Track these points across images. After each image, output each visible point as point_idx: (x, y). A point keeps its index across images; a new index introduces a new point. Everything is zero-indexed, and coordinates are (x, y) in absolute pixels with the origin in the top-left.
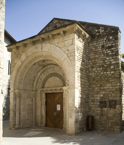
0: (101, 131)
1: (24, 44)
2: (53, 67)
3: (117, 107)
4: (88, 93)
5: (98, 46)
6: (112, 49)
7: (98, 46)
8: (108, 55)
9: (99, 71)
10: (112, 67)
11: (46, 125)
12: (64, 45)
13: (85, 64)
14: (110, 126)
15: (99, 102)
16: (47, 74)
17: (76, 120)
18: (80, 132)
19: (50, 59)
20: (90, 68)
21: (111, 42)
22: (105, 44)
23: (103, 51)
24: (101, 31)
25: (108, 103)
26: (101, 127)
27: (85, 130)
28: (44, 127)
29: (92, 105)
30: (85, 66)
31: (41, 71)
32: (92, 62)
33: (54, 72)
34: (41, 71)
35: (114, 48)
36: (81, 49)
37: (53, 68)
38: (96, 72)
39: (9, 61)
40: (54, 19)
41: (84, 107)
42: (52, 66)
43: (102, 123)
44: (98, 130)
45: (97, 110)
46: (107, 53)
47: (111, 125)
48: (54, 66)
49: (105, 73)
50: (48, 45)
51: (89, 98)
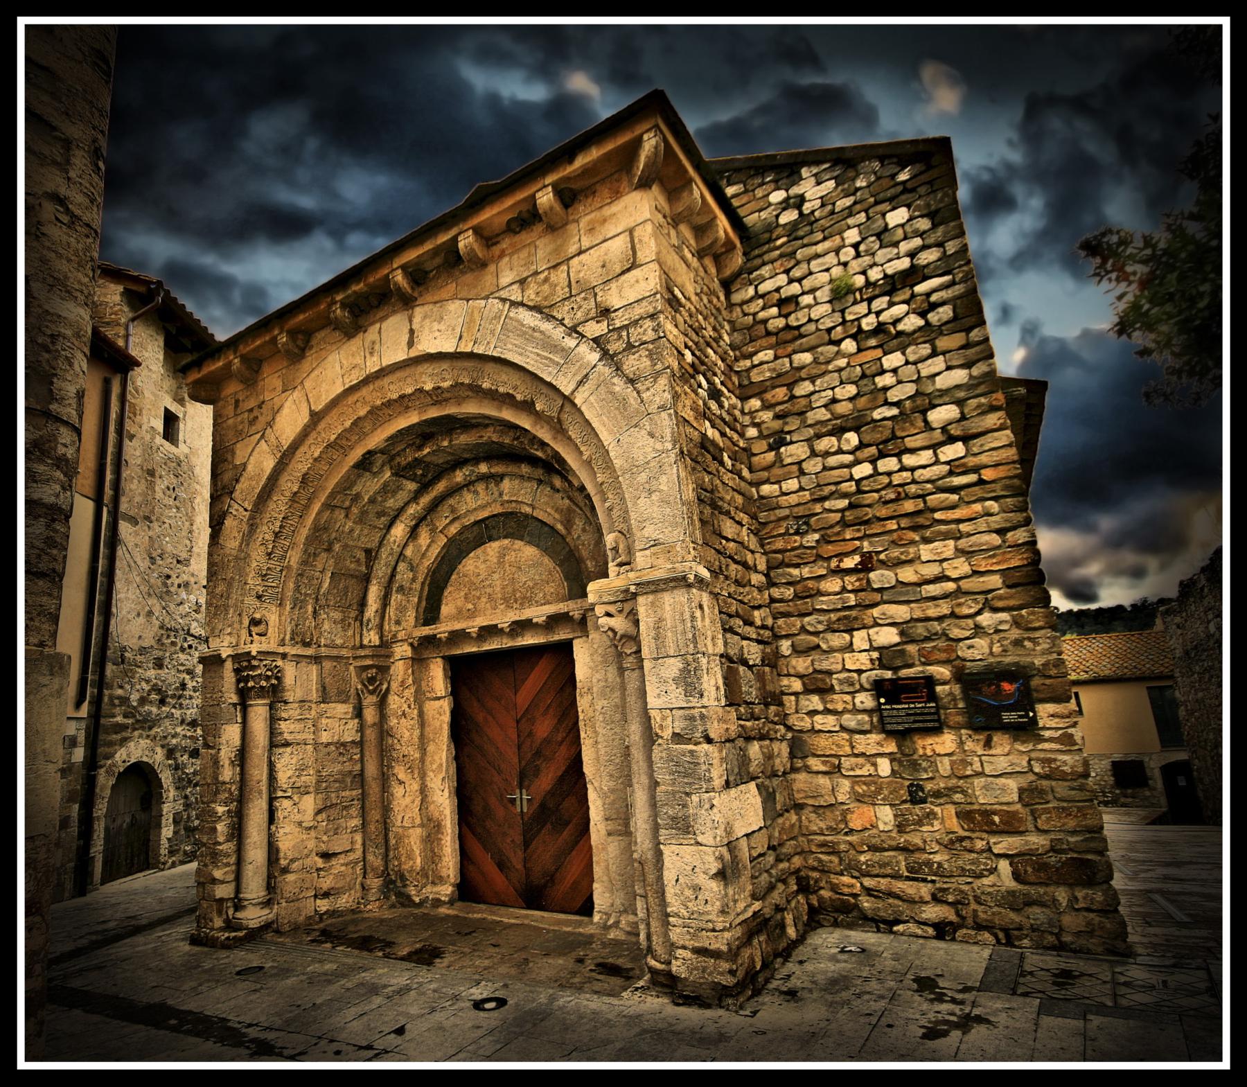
3: (1052, 723)
5: (803, 293)
6: (921, 288)
9: (833, 461)
10: (942, 414)
14: (1011, 893)
21: (905, 247)
23: (849, 317)
26: (928, 898)
28: (451, 902)
29: (818, 718)
32: (766, 406)
45: (863, 755)
46: (880, 324)
47: (1016, 876)
49: (889, 464)
51: (782, 662)
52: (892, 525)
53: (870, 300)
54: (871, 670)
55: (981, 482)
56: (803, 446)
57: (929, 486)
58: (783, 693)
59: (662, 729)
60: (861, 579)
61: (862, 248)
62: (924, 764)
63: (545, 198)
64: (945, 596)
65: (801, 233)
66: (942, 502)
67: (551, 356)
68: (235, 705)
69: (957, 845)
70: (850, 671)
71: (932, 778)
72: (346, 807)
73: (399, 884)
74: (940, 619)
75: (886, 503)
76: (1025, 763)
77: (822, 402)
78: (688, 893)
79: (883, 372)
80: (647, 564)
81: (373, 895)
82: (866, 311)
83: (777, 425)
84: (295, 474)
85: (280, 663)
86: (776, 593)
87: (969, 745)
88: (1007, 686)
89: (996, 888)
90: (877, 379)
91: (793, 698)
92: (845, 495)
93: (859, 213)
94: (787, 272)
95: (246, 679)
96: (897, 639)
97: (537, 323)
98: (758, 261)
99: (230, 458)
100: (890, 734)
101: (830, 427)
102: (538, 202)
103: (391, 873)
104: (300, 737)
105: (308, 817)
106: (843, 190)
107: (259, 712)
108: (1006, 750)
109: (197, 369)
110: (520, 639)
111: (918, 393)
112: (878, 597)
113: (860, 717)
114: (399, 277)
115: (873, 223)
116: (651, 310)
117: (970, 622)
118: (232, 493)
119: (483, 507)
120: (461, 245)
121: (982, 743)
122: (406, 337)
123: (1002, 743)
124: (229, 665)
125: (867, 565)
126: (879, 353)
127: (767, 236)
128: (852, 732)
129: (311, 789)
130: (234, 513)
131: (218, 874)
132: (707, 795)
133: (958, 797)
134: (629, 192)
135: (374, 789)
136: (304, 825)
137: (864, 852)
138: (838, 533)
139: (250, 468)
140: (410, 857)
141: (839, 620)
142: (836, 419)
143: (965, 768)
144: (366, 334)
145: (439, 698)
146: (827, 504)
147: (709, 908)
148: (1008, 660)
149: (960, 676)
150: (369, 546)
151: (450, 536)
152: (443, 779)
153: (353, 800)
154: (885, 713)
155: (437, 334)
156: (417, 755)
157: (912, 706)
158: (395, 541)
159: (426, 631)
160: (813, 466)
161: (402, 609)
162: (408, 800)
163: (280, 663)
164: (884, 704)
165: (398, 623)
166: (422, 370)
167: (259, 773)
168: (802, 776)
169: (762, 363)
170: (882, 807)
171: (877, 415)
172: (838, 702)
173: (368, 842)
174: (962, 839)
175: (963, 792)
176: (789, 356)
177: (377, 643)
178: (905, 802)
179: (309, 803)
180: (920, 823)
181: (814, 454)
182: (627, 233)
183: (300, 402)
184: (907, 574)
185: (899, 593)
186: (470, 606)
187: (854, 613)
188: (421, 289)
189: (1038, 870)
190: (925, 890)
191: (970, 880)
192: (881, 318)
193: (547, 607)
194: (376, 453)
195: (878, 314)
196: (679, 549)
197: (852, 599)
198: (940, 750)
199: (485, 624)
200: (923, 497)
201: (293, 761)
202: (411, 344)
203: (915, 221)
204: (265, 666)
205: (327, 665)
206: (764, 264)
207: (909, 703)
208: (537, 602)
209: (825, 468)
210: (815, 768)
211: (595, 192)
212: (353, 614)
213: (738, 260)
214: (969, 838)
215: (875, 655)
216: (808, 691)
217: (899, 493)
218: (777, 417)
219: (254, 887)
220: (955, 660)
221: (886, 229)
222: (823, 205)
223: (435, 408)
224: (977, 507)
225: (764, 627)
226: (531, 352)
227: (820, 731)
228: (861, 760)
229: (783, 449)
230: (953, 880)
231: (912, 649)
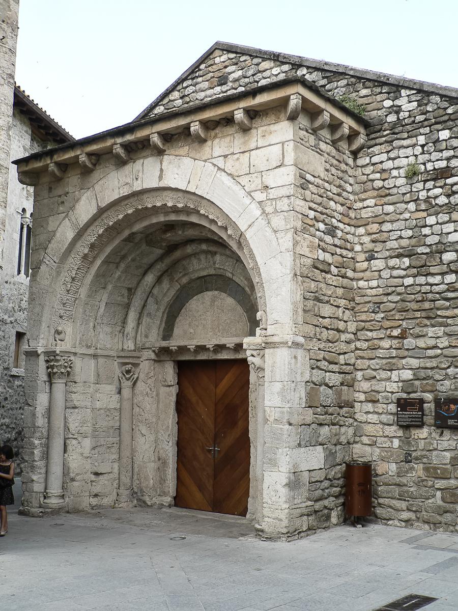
0: (403, 524)
4: (349, 364)
5: (394, 168)
8: (431, 207)
9: (396, 273)
11: (179, 501)
13: (337, 242)
14: (439, 507)
15: (395, 401)
16: (185, 280)
17: (292, 477)
18: (309, 529)
21: (446, 154)
22: (421, 159)
23: (414, 190)
25: (432, 405)
26: (405, 508)
27: (334, 520)
28: (170, 506)
29: (370, 416)
30: (338, 251)
31: (161, 266)
34: (161, 266)
36: (317, 180)
39: (24, 210)
41: (334, 424)
42: (204, 247)
43: (408, 492)
44: (390, 522)
46: (428, 197)
47: (443, 499)
49: (421, 280)
50: (187, 161)
51: (356, 383)
52: (418, 314)
53: (425, 181)
54: (398, 392)
56: (382, 262)
57: (438, 295)
59: (269, 417)
60: (400, 343)
61: (425, 148)
62: (413, 443)
63: (239, 115)
64: (436, 357)
65: (397, 131)
66: (442, 305)
67: (236, 206)
68: (45, 382)
69: (421, 484)
70: (388, 392)
71: (416, 451)
72: (109, 447)
73: (139, 494)
74: (432, 368)
76: (454, 445)
78: (273, 493)
79: (426, 226)
81: (124, 498)
82: (422, 188)
83: (370, 246)
84: (87, 243)
85: (72, 358)
86: (358, 344)
87: (434, 435)
88: (452, 407)
89: (434, 504)
90: (423, 229)
91: (359, 404)
92: (399, 294)
93: (426, 127)
95: (52, 367)
96: (411, 377)
97: (231, 184)
98: (373, 142)
99: (45, 226)
100: (401, 426)
101: (396, 253)
102: (235, 116)
103: (135, 488)
104: (83, 404)
105: (87, 452)
106: (420, 110)
107: (59, 386)
108: (448, 438)
109: (25, 164)
110: (220, 355)
111: (440, 242)
112: (406, 353)
113: (389, 417)
115: (433, 134)
116: (288, 194)
117: (444, 371)
118: (46, 249)
119: (203, 269)
120: (192, 129)
121: (439, 434)
122: (158, 173)
124: (42, 358)
125: (402, 336)
127: (379, 127)
130: (47, 262)
131: (35, 478)
132: (285, 449)
133: (425, 460)
135: (126, 438)
136: (84, 455)
137: (381, 486)
138: (392, 315)
139: (58, 235)
140: (146, 478)
141: (386, 364)
142: (401, 248)
143: (430, 446)
144: (134, 165)
145: (169, 386)
146: (390, 298)
147: (280, 500)
149: (437, 401)
150: (130, 286)
151: (182, 284)
153: (113, 444)
154: (399, 416)
155: (177, 176)
156: (154, 420)
157: (411, 413)
158: (147, 284)
159: (164, 344)
160: (386, 274)
161: (149, 328)
162: (147, 446)
163: (72, 358)
164: (400, 411)
166: (166, 194)
167: (58, 423)
169: (368, 207)
170: (392, 463)
173: (121, 469)
174: (423, 481)
175: (428, 458)
177: (133, 349)
178: (402, 461)
179: (87, 443)
180: (407, 472)
181: (388, 267)
182: (281, 144)
183: (92, 199)
184: (421, 343)
185: (417, 352)
186: (192, 331)
187: (394, 361)
188: (168, 144)
189: (452, 496)
190: (404, 505)
191: (423, 500)
192: (429, 194)
193: (235, 338)
194: (137, 233)
195: (429, 190)
196: (287, 327)
197: (394, 353)
199: (199, 344)
201: (79, 418)
202: (161, 178)
203: (452, 140)
204: (64, 360)
205: (101, 360)
206: (376, 145)
207: (410, 412)
208: (231, 333)
210: (365, 442)
211: (267, 114)
212: (119, 328)
213: (361, 140)
214: (426, 480)
215: (400, 384)
216: (367, 401)
217: (423, 298)
219: (55, 488)
220: (435, 391)
221: (437, 141)
222: (410, 116)
223: (173, 214)
226: (227, 201)
227: (370, 423)
228: (386, 439)
229: (372, 261)
230: (417, 500)
231: (417, 383)
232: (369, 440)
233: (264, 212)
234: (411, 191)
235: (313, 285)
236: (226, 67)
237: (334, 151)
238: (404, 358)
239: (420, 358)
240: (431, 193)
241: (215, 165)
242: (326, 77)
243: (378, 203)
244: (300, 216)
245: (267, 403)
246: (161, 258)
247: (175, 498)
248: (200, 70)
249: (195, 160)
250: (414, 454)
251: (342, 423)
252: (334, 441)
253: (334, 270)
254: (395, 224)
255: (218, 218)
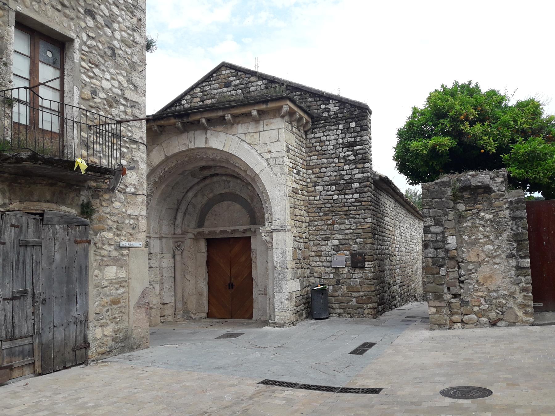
0: (338, 315)
1: (160, 126)
2: (227, 180)
3: (368, 266)
5: (327, 141)
6: (356, 148)
7: (327, 141)
8: (347, 162)
9: (329, 193)
10: (356, 185)
11: (210, 315)
12: (260, 140)
16: (211, 195)
19: (224, 165)
20: (310, 185)
21: (353, 135)
23: (337, 152)
24: (334, 108)
27: (304, 316)
29: (318, 263)
30: (301, 182)
31: (197, 188)
32: (313, 173)
33: (227, 191)
35: (359, 147)
37: (226, 183)
38: (323, 193)
40: (224, 66)
42: (224, 178)
45: (327, 273)
46: (345, 156)
47: (357, 302)
48: (229, 179)
53: (343, 148)
55: (361, 205)
58: (309, 256)
63: (254, 113)
74: (348, 239)
75: (340, 207)
77: (328, 175)
79: (343, 170)
80: (276, 225)
83: (315, 179)
86: (310, 228)
90: (342, 172)
92: (330, 203)
94: (323, 132)
98: (315, 126)
111: (351, 179)
112: (335, 232)
114: (204, 121)
116: (282, 156)
117: (354, 241)
120: (226, 118)
123: (357, 270)
125: (332, 224)
126: (343, 164)
128: (325, 267)
129: (158, 282)
133: (347, 284)
134: (278, 118)
145: (202, 252)
146: (326, 205)
148: (361, 251)
152: (204, 279)
160: (323, 193)
165: (188, 226)
168: (312, 278)
169: (313, 160)
171: (340, 182)
172: (323, 259)
176: (321, 159)
181: (324, 190)
184: (343, 227)
186: (216, 222)
187: (329, 236)
195: (345, 153)
198: (344, 272)
200: (348, 207)
209: (326, 195)
215: (333, 247)
218: (316, 177)
221: (349, 127)
222: (335, 114)
224: (360, 212)
225: (306, 238)
231: (341, 246)
232: (318, 275)
233: (269, 164)
234: (336, 153)
235: (293, 200)
236: (229, 77)
237: (298, 132)
238: (334, 234)
239: (342, 234)
240: (346, 154)
241: (239, 138)
242: (289, 89)
243: (319, 158)
244: (287, 166)
245: (275, 259)
246: (198, 183)
247: (208, 313)
248: (213, 77)
249: (227, 134)
250: (341, 281)
251: (305, 267)
252: (302, 276)
253: (300, 192)
254: (327, 169)
255: (241, 165)
